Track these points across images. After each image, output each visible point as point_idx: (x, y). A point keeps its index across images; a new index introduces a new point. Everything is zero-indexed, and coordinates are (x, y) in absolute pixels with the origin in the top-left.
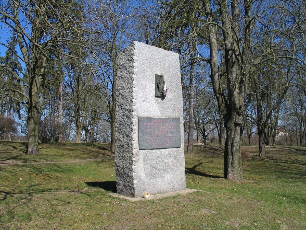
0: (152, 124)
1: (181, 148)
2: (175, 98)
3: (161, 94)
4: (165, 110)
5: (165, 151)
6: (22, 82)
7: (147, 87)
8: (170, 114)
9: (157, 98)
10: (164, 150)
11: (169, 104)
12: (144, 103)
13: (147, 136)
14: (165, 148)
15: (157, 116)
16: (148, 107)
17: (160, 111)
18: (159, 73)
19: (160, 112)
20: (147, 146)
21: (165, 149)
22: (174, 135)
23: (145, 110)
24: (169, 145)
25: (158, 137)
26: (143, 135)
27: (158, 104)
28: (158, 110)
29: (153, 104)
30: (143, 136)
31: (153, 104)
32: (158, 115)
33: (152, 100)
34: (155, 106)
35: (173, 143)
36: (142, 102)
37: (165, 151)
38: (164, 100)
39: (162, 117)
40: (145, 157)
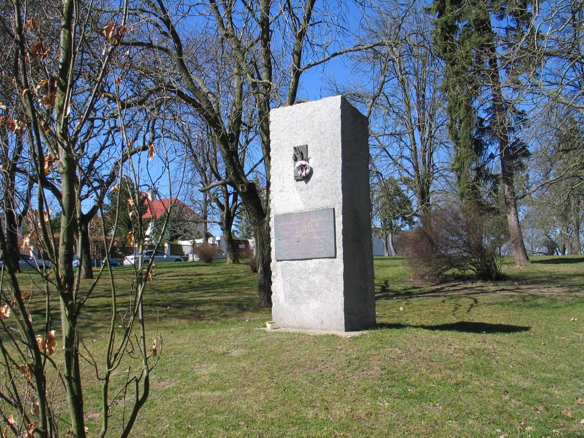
0: (291, 223)
1: (337, 259)
4: (310, 198)
7: (285, 170)
12: (283, 194)
14: (311, 259)
17: (302, 201)
18: (299, 143)
21: (310, 261)
22: (322, 237)
24: (313, 255)
25: (298, 241)
35: (322, 249)
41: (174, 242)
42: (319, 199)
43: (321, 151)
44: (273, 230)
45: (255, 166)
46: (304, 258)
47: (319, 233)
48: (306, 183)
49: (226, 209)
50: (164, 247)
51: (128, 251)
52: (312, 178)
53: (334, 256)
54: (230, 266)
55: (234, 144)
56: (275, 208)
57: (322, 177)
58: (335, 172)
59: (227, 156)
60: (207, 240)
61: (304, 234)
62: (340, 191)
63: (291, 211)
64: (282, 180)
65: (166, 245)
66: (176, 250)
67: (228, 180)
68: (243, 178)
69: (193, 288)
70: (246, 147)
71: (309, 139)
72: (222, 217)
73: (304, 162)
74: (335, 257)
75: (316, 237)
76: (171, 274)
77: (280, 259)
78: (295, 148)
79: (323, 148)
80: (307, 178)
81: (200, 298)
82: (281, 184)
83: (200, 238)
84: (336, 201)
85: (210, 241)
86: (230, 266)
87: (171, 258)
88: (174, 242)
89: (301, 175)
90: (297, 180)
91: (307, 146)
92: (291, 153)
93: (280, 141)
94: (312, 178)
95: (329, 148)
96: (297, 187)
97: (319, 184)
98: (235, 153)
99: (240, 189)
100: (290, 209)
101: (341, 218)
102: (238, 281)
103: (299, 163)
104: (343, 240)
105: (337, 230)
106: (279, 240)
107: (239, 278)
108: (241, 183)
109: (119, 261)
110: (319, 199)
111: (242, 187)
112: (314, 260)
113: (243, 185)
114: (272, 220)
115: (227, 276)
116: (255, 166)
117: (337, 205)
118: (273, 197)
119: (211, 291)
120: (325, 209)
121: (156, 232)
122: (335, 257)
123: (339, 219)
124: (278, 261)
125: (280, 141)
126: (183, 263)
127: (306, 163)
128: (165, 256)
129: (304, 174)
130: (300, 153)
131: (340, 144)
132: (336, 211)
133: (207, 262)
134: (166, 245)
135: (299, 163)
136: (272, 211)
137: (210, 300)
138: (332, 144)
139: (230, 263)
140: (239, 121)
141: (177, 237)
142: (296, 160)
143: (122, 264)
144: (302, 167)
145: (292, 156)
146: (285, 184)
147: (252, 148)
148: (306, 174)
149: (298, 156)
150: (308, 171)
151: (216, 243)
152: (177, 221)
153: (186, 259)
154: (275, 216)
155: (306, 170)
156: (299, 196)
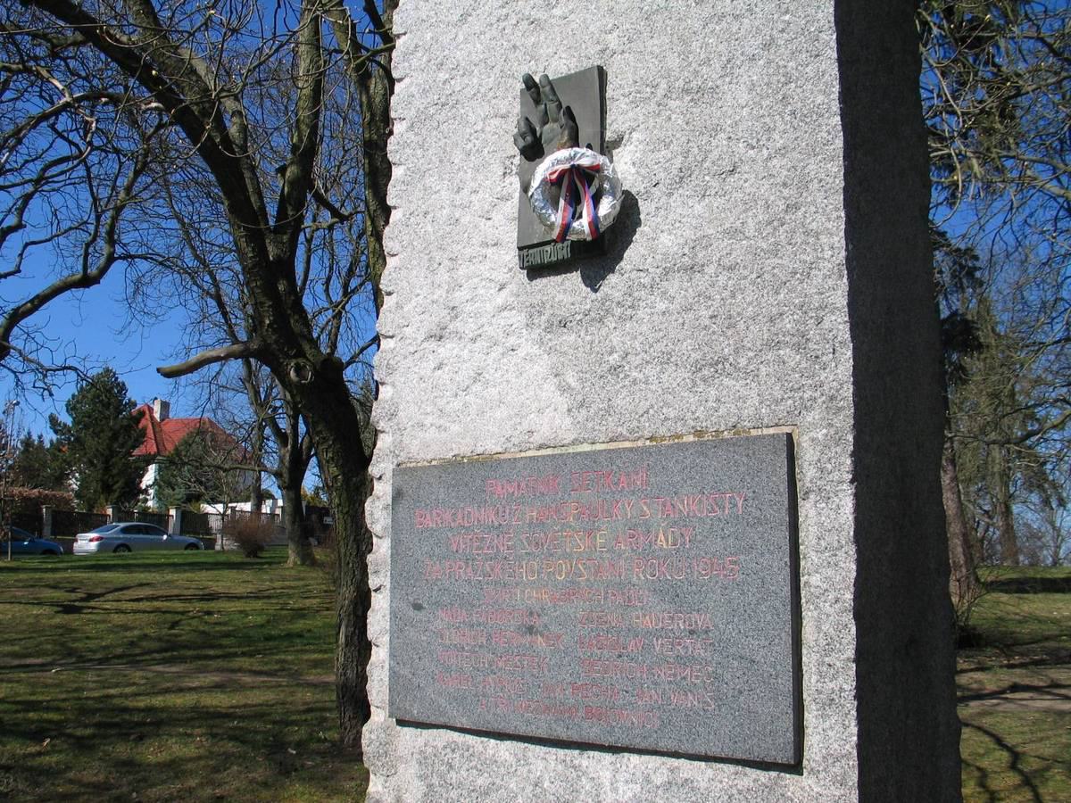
0: (491, 518)
1: (806, 780)
2: (733, 233)
3: (585, 244)
4: (615, 370)
5: (606, 776)
6: (457, 294)
7: (465, 220)
8: (671, 402)
9: (541, 282)
10: (598, 765)
11: (661, 306)
12: (447, 350)
13: (440, 621)
14: (614, 749)
15: (537, 439)
16: (466, 372)
17: (564, 389)
18: (557, 65)
19: (563, 402)
20: (442, 701)
21: (608, 758)
22: (700, 621)
23: (441, 403)
24: (632, 724)
25: (531, 630)
26: (418, 607)
27: (549, 329)
28: (550, 386)
29: (512, 341)
30: (412, 613)
31: (512, 341)
32: (543, 433)
33: (504, 308)
34: (529, 359)
35: (691, 701)
36: (432, 345)
37: (606, 776)
38: (612, 279)
39: (586, 448)
40: (430, 786)
41: (191, 508)
42: (675, 376)
43: (698, 93)
44: (382, 550)
45: (362, 350)
46: (562, 733)
47: (674, 596)
48: (593, 282)
49: (290, 441)
50: (169, 516)
51: (90, 522)
52: (629, 254)
53: (786, 756)
54: (293, 572)
55: (285, 238)
56: (400, 430)
57: (702, 242)
58: (792, 207)
59: (254, 266)
60: (258, 506)
61: (571, 591)
62: (839, 324)
63: (491, 446)
64: (443, 276)
65: (173, 512)
66: (194, 523)
67: (254, 346)
68: (306, 347)
69: (171, 650)
70: (343, 308)
71: (613, 41)
72: (282, 460)
73: (586, 158)
74: (796, 767)
75: (651, 616)
76: (148, 592)
77: (415, 713)
78: (529, 83)
79: (712, 73)
80: (596, 255)
81: (158, 701)
82: (440, 293)
83: (246, 500)
84: (812, 393)
85: (266, 508)
86: (293, 572)
87: (178, 541)
88: (191, 508)
89: (566, 228)
90: (536, 271)
91: (602, 73)
92: (512, 105)
93: (443, 76)
94: (633, 255)
95: (755, 73)
96: (534, 310)
97: (674, 285)
98: (285, 266)
99: (292, 374)
100: (489, 435)
101: (848, 504)
102: (300, 625)
103: (554, 161)
104: (864, 657)
105: (812, 580)
106: (411, 607)
107: (303, 617)
108: (295, 356)
109: (63, 542)
110: (675, 376)
111: (299, 370)
112: (635, 759)
113: (301, 361)
114: (382, 490)
115: (271, 607)
116: (362, 350)
117: (812, 417)
118: (391, 370)
119: (214, 664)
120: (719, 442)
121: (162, 483)
122: (796, 767)
123: (831, 516)
124: (401, 723)
125: (443, 76)
126: (201, 556)
127: (601, 159)
128: (165, 537)
129: (583, 225)
130: (558, 112)
131: (830, 38)
132: (808, 455)
133: (248, 556)
134: (173, 512)
135: (554, 161)
136: (384, 442)
137: (195, 709)
138: (766, 46)
139: (295, 563)
140: (303, 183)
141: (198, 498)
142: (533, 150)
143: (70, 551)
144: (576, 184)
145: (513, 126)
146: (460, 295)
147: (355, 312)
148: (594, 223)
149: (547, 131)
150: (607, 207)
151: (278, 511)
152: (201, 461)
153: (210, 544)
154: (400, 470)
155: (596, 200)
156: (542, 366)
